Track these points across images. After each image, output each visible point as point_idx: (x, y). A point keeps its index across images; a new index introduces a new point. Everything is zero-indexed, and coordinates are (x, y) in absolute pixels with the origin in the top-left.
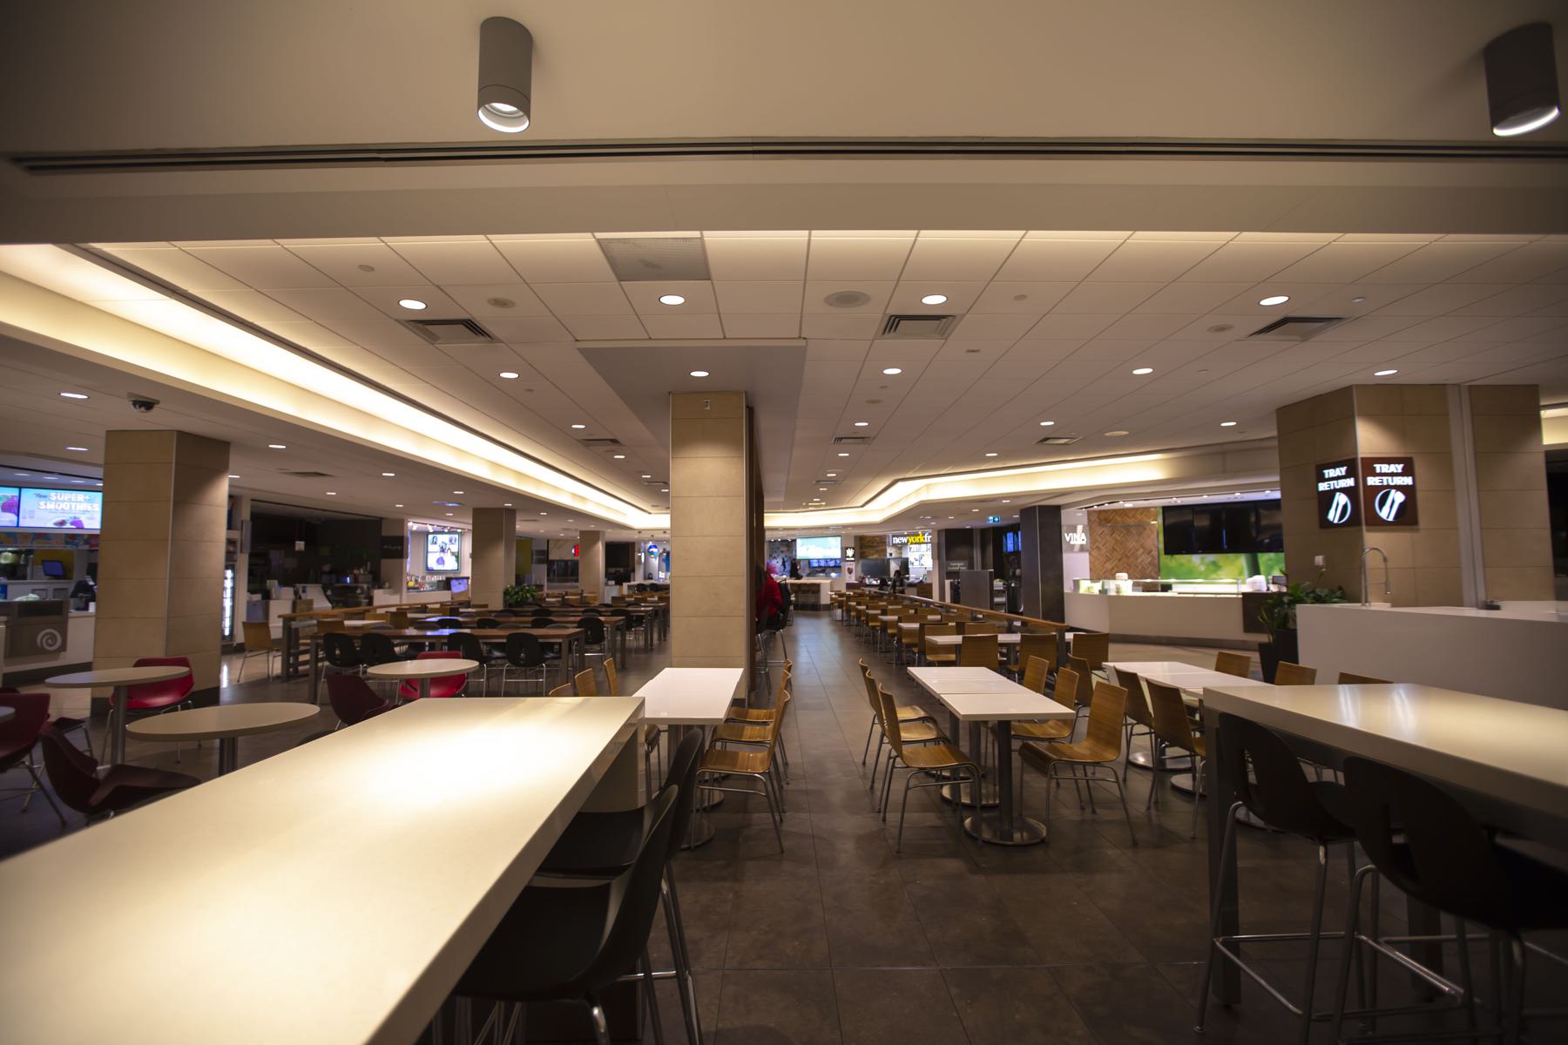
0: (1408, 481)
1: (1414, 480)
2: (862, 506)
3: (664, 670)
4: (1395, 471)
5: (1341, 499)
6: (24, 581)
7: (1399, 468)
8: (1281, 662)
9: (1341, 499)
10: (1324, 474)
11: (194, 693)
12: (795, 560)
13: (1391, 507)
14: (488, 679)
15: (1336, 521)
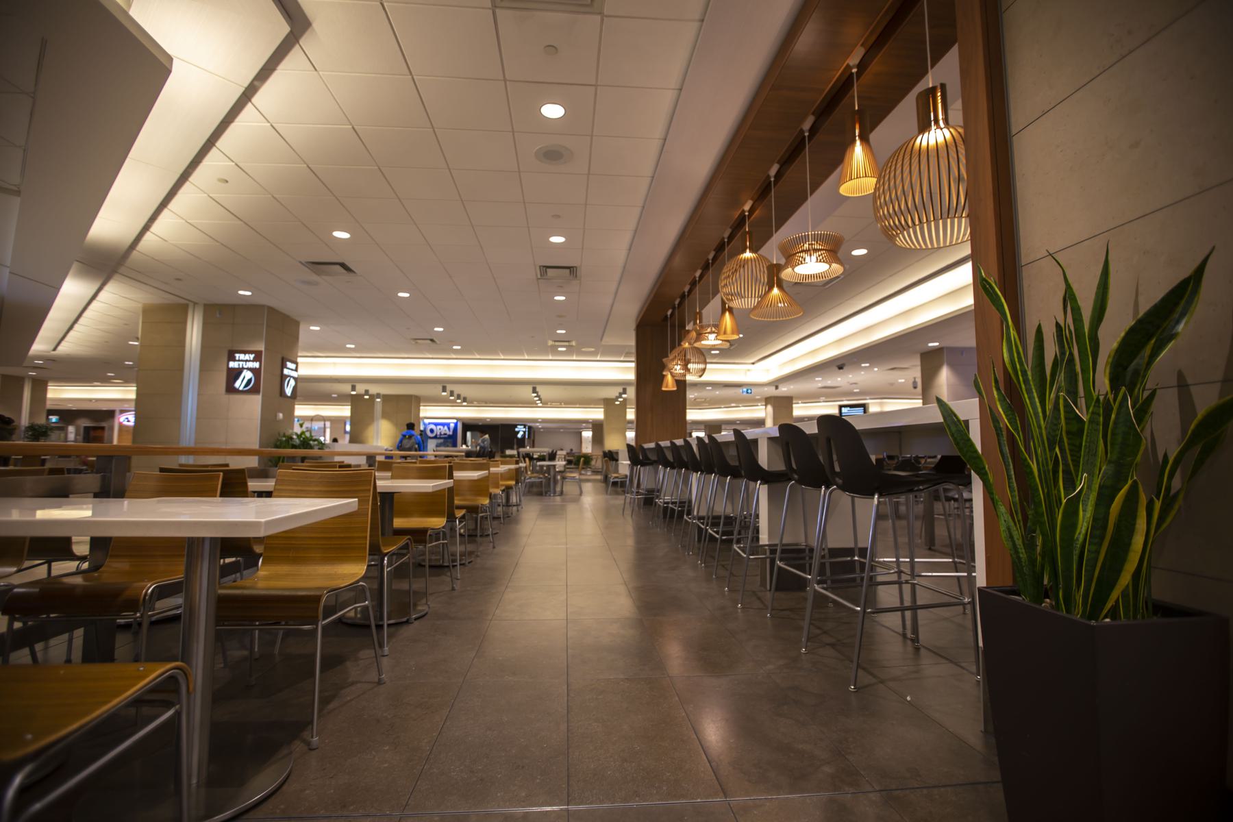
0: (256, 365)
1: (228, 364)
2: (753, 363)
4: (249, 359)
5: (248, 375)
9: (248, 375)
10: (235, 357)
11: (773, 286)
12: (29, 427)
13: (242, 381)
15: (241, 388)
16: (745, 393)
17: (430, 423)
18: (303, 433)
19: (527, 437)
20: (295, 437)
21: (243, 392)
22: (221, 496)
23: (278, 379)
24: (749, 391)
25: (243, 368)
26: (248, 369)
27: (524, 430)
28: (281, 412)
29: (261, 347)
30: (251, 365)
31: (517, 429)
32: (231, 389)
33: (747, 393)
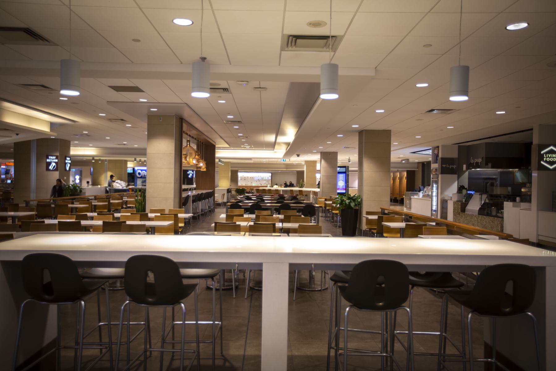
0: (57, 161)
1: (46, 160)
3: (127, 260)
6: (389, 211)
7: (192, 171)
8: (59, 215)
9: (54, 164)
14: (474, 162)
16: (282, 161)
17: (138, 170)
18: (74, 184)
19: (194, 177)
20: (70, 186)
21: (52, 170)
22: (187, 185)
23: (64, 164)
24: (285, 160)
25: (52, 162)
26: (54, 162)
27: (192, 173)
28: (66, 177)
29: (58, 154)
30: (55, 160)
31: (188, 173)
32: (48, 169)
33: (283, 161)
